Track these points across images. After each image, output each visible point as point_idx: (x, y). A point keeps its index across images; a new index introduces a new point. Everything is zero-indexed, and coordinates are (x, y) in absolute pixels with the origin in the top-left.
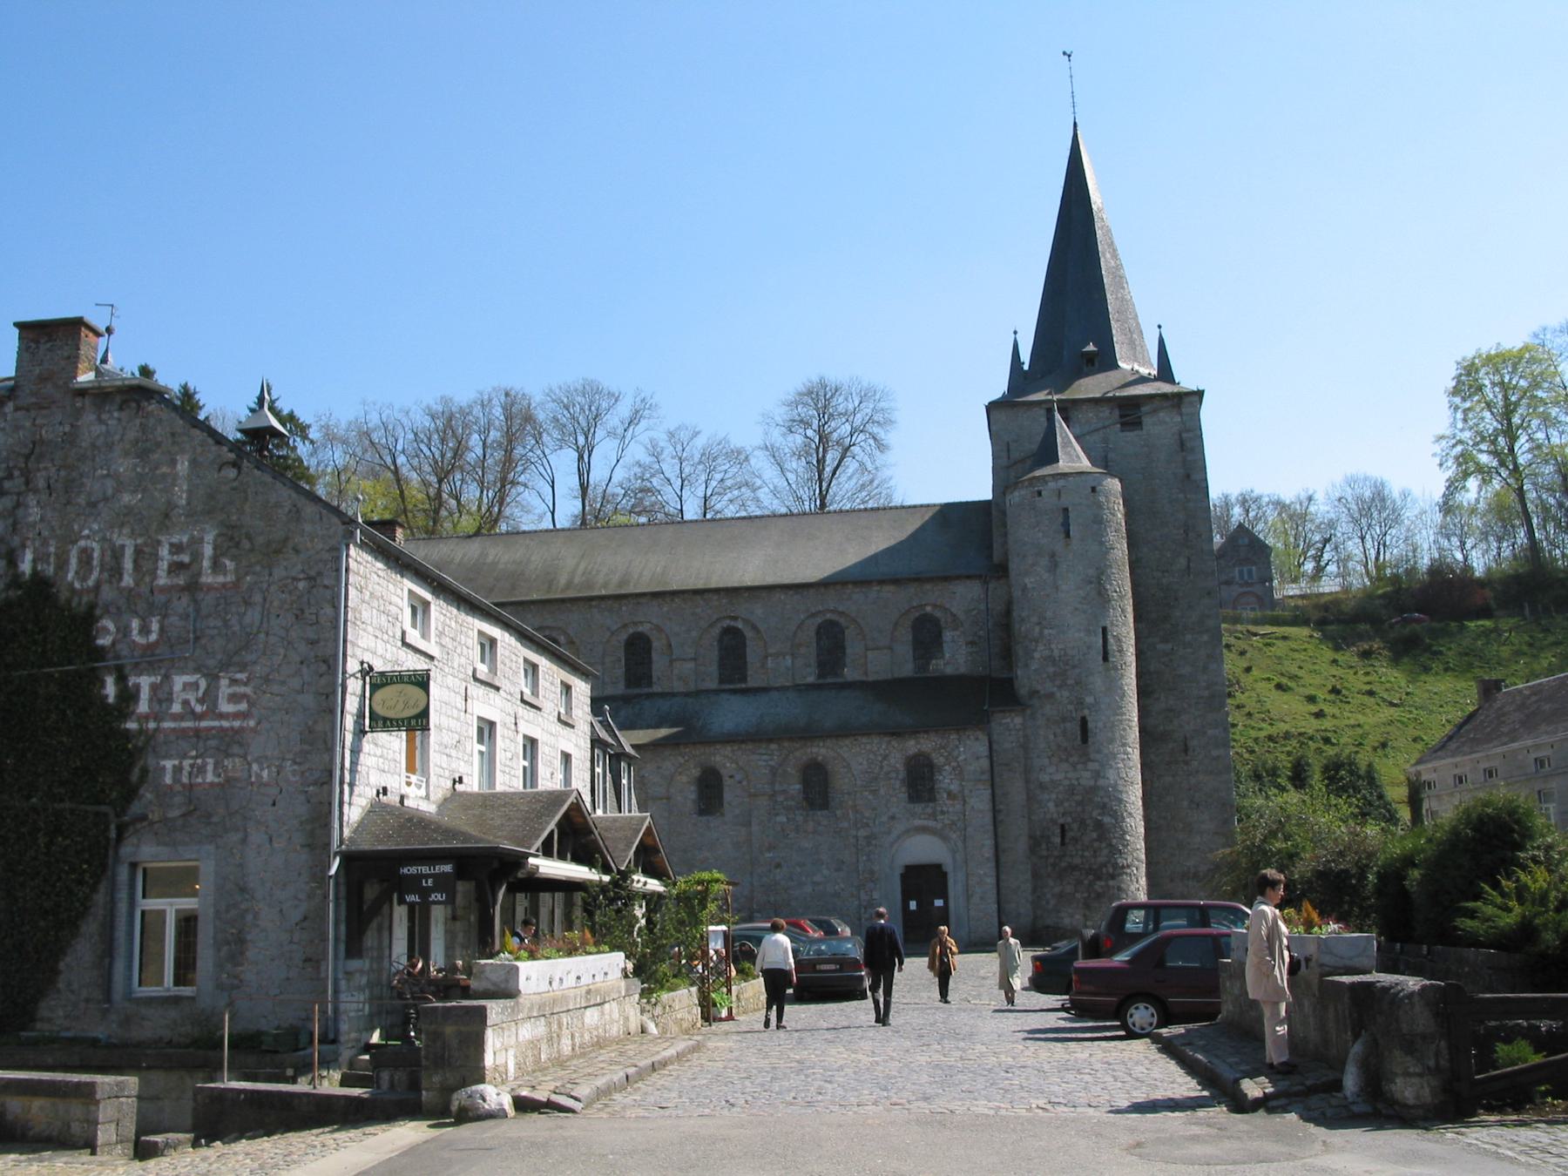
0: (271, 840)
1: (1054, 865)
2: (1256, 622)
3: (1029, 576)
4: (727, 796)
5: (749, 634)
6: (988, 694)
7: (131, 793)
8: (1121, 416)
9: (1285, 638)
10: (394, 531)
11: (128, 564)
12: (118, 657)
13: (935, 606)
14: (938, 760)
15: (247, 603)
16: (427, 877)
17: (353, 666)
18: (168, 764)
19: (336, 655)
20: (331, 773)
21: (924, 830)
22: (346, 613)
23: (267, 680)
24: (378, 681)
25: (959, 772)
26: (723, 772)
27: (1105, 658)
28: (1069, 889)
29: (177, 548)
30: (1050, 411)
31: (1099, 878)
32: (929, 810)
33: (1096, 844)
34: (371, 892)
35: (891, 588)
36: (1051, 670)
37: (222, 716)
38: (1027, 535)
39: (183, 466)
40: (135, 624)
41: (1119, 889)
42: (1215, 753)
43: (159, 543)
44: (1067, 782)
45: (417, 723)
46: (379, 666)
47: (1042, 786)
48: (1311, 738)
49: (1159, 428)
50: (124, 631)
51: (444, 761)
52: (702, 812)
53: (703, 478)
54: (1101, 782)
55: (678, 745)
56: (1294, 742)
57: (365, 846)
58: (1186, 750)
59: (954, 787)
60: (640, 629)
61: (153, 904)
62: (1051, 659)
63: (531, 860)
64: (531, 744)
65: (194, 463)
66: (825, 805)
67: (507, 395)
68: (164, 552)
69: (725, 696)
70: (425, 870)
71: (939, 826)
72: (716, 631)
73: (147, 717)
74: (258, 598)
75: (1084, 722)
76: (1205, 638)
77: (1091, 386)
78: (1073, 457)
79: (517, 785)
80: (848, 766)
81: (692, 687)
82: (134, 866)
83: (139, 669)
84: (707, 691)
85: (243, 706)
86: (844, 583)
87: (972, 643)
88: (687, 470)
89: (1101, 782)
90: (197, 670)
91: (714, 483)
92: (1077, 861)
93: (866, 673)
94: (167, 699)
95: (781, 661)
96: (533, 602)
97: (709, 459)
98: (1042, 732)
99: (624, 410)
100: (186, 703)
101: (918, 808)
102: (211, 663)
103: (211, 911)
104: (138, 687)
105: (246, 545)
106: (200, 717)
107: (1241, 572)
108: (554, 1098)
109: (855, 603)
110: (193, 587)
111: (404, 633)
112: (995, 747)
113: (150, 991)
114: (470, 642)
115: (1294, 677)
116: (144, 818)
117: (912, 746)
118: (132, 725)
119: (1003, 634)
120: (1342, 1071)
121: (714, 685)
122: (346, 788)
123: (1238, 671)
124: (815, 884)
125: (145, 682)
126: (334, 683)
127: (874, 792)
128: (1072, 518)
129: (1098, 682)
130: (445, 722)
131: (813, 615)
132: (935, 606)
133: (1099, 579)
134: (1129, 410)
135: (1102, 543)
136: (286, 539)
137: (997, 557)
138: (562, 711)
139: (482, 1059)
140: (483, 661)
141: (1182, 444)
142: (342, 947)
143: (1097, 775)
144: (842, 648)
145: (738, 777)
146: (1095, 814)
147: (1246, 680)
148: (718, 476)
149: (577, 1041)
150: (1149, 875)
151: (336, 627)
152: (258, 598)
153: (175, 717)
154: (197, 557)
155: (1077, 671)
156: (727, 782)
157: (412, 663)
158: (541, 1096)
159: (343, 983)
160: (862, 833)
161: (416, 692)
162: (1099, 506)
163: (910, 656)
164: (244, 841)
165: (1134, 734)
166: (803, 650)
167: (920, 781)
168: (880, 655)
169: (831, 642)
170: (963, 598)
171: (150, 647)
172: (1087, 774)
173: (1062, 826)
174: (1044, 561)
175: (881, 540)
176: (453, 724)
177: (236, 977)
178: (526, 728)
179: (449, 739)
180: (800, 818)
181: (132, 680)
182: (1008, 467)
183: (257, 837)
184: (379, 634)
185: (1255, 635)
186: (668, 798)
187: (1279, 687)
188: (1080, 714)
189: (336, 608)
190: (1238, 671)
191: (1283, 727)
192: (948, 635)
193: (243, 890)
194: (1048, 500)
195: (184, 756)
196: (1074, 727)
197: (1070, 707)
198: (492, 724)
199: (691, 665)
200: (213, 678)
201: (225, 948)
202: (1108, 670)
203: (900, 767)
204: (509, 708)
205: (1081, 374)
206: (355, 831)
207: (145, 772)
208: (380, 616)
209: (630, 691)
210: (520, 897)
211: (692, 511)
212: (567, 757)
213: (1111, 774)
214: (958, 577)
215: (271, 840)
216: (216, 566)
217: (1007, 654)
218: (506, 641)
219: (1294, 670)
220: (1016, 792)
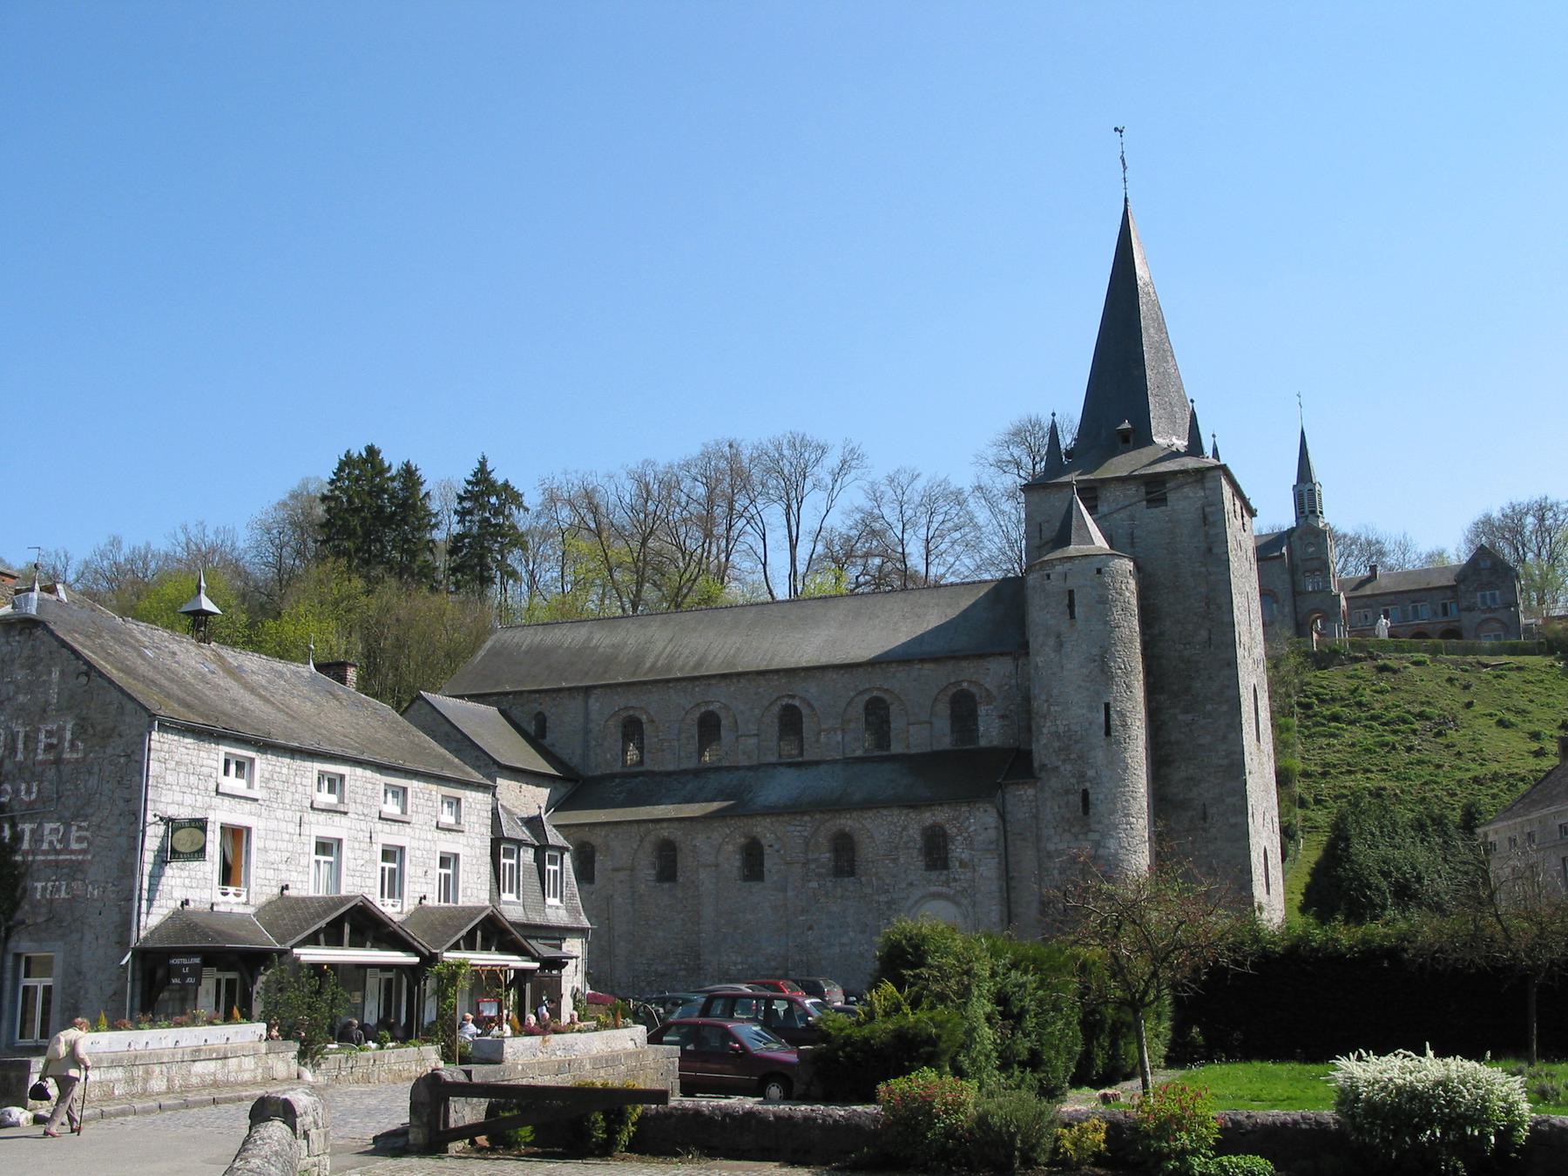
2: (1493, 652)
4: (767, 864)
5: (805, 711)
6: (1017, 763)
7: (16, 905)
8: (1147, 493)
9: (1520, 669)
11: (20, 746)
12: (12, 810)
13: (970, 682)
14: (951, 830)
15: (90, 773)
18: (39, 885)
23: (99, 826)
26: (763, 842)
27: (1108, 733)
29: (50, 734)
32: (943, 878)
35: (931, 666)
36: (1056, 744)
37: (72, 852)
38: (1042, 615)
39: (55, 675)
40: (23, 787)
42: (1232, 820)
43: (39, 730)
47: (1049, 856)
48: (1522, 780)
50: (16, 792)
52: (747, 878)
53: (924, 520)
54: (1101, 852)
55: (724, 817)
56: (1502, 784)
57: (150, 945)
58: (1205, 818)
61: (30, 982)
62: (1057, 736)
65: (62, 673)
66: (852, 873)
67: (731, 446)
68: (42, 736)
69: (782, 769)
70: (185, 961)
72: (776, 709)
73: (26, 853)
74: (96, 769)
75: (1085, 794)
76: (1225, 708)
77: (1122, 465)
80: (872, 837)
81: (754, 762)
82: (18, 956)
83: (24, 818)
84: (768, 765)
85: (85, 845)
86: (889, 663)
87: (1002, 717)
88: (909, 513)
89: (1101, 852)
90: (59, 820)
91: (935, 525)
94: (42, 839)
95: (835, 735)
96: (620, 685)
97: (929, 504)
99: (832, 460)
100: (51, 843)
101: (934, 875)
102: (67, 814)
104: (23, 831)
105: (91, 731)
106: (58, 853)
107: (1483, 597)
110: (58, 762)
113: (27, 1042)
115: (1521, 712)
116: (23, 922)
117: (928, 818)
118: (18, 858)
119: (1023, 712)
122: (144, 903)
123: (1456, 707)
124: (844, 945)
125: (27, 828)
126: (137, 831)
127: (895, 860)
128: (1083, 600)
129: (1099, 756)
131: (860, 693)
132: (970, 682)
133: (1103, 657)
134: (1155, 487)
135: (1106, 623)
136: (114, 729)
141: (1205, 518)
143: (1097, 845)
144: (888, 722)
147: (1463, 715)
148: (941, 518)
152: (96, 769)
153: (46, 853)
154: (61, 739)
156: (767, 851)
160: (883, 898)
161: (198, 833)
162: (1105, 587)
163: (947, 730)
164: (81, 939)
166: (852, 726)
167: (936, 851)
168: (921, 730)
169: (877, 713)
170: (994, 674)
171: (31, 803)
174: (1052, 642)
175: (933, 617)
181: (20, 826)
182: (1039, 547)
183: (89, 937)
185: (1486, 666)
186: (717, 866)
187: (1501, 723)
190: (1456, 707)
191: (1495, 767)
192: (982, 710)
193: (79, 973)
194: (1056, 583)
195: (48, 880)
196: (1076, 799)
199: (753, 741)
200: (68, 826)
202: (1110, 744)
205: (1114, 453)
206: (152, 933)
207: (25, 890)
211: (782, 592)
216: (73, 745)
219: (1522, 703)
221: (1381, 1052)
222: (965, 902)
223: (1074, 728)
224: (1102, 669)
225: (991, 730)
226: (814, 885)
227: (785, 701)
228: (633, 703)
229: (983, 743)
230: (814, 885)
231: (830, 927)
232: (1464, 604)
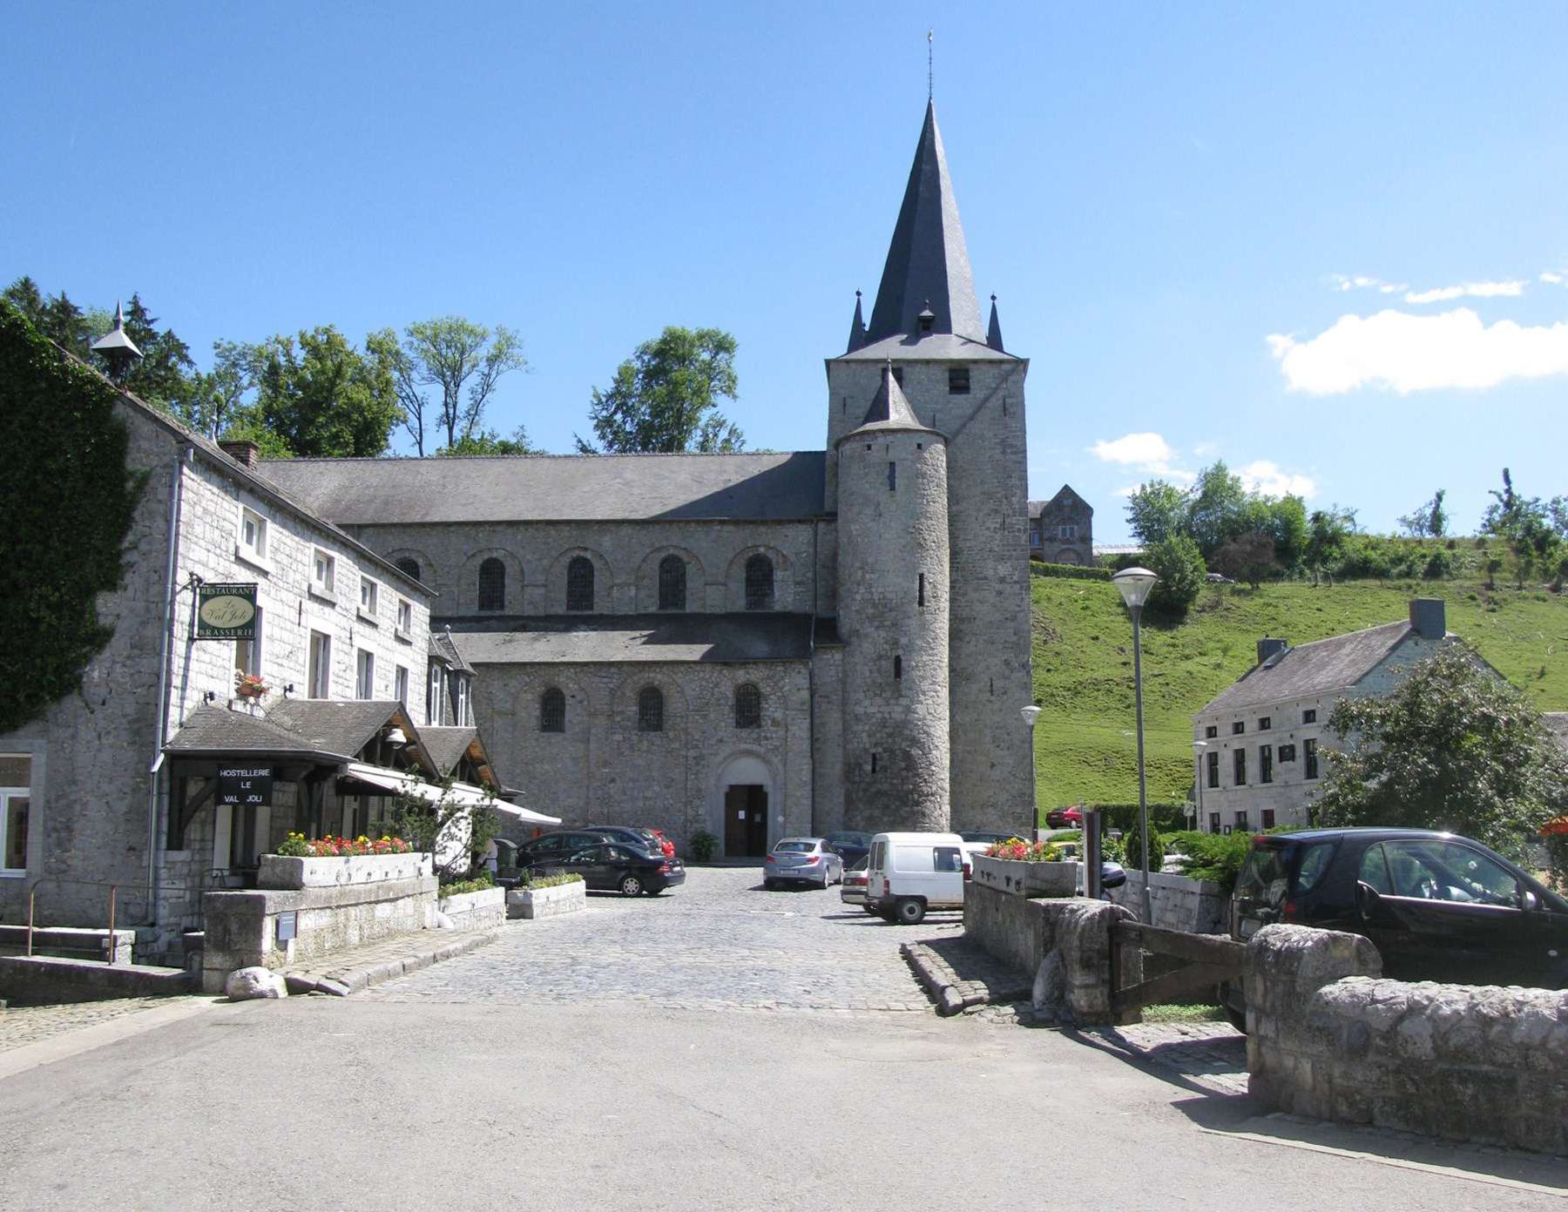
0: (99, 737)
1: (865, 790)
3: (856, 524)
4: (569, 715)
5: (597, 564)
6: (815, 630)
10: (248, 453)
14: (765, 689)
16: (246, 779)
17: (182, 578)
19: (167, 567)
20: (158, 676)
21: (749, 753)
22: (178, 527)
24: (207, 592)
25: (784, 699)
26: (565, 691)
27: (921, 603)
30: (885, 371)
31: (905, 804)
33: (904, 773)
34: (193, 789)
38: (859, 483)
41: (924, 815)
45: (247, 634)
46: (210, 578)
47: (857, 719)
49: (984, 396)
51: (275, 670)
59: (778, 715)
60: (495, 555)
63: (352, 766)
64: (366, 658)
66: (658, 727)
70: (244, 773)
71: (762, 750)
72: (566, 560)
75: (898, 660)
78: (900, 414)
79: (352, 694)
80: (682, 692)
81: (541, 612)
86: (671, 522)
92: (886, 787)
93: (704, 606)
99: (485, 350)
101: (744, 733)
103: (42, 801)
108: (324, 982)
111: (237, 548)
112: (816, 680)
114: (306, 560)
117: (741, 676)
119: (828, 573)
120: (1032, 981)
121: (561, 610)
124: (645, 798)
127: (704, 717)
129: (913, 623)
130: (277, 633)
131: (659, 550)
134: (959, 376)
137: (828, 506)
138: (401, 628)
139: (260, 945)
140: (319, 578)
142: (164, 838)
143: (908, 710)
145: (579, 698)
146: (904, 745)
149: (366, 932)
150: (953, 804)
151: (168, 540)
156: (569, 701)
157: (243, 576)
158: (312, 979)
159: (163, 873)
160: (692, 753)
161: (243, 604)
163: (742, 593)
164: (73, 737)
165: (943, 675)
166: (646, 582)
167: (748, 709)
170: (791, 544)
172: (900, 709)
173: (874, 755)
174: (869, 511)
176: (286, 636)
177: (64, 862)
178: (360, 642)
179: (283, 649)
180: (635, 738)
184: (210, 547)
189: (168, 522)
192: (778, 575)
196: (888, 665)
198: (327, 637)
199: (542, 591)
201: (54, 835)
204: (344, 622)
208: (208, 531)
209: (483, 613)
210: (349, 799)
212: (402, 673)
213: (921, 710)
214: (790, 522)
215: (99, 737)
217: (833, 596)
218: (343, 562)
220: (833, 722)
222: (775, 760)
223: (889, 596)
224: (918, 546)
225: (786, 595)
226: (618, 737)
227: (575, 554)
228: (409, 545)
230: (618, 737)
231: (634, 780)
232: (1046, 535)
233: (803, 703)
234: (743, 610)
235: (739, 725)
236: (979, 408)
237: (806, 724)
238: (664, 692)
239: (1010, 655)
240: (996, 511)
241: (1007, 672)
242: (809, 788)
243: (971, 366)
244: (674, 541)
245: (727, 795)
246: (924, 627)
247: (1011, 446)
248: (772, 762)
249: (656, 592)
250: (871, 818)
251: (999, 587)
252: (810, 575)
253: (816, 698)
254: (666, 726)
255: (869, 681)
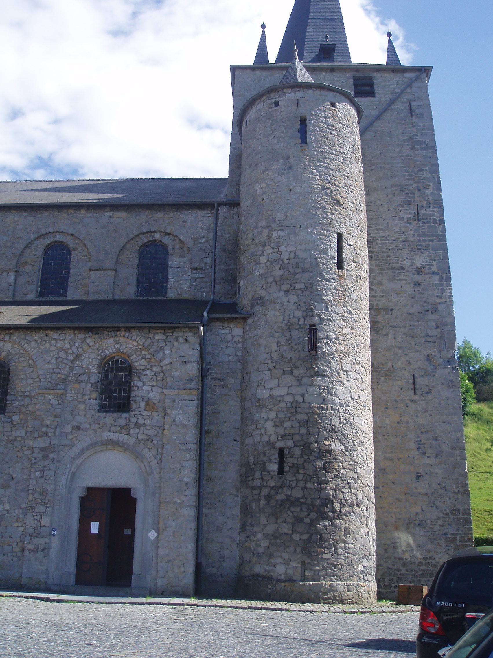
1: (268, 498)
14: (139, 363)
27: (340, 265)
28: (285, 529)
32: (122, 422)
41: (347, 532)
44: (289, 399)
47: (260, 404)
59: (154, 396)
71: (132, 441)
75: (313, 330)
92: (297, 493)
98: (262, 342)
101: (109, 418)
109: (90, 226)
117: (109, 345)
131: (42, 236)
155: (307, 275)
160: (40, 443)
163: (133, 280)
166: (28, 268)
167: (116, 391)
173: (281, 451)
188: (309, 322)
192: (174, 261)
197: (298, 314)
203: (94, 369)
217: (233, 280)
220: (229, 411)
221: (226, 599)
222: (148, 454)
223: (301, 255)
225: (181, 282)
229: (171, 295)
233: (191, 380)
234: (133, 297)
235: (104, 408)
236: (385, 110)
237: (192, 407)
238: (12, 366)
239: (433, 351)
240: (409, 203)
241: (430, 369)
242: (192, 491)
243: (375, 75)
244: (63, 226)
245: (83, 500)
246: (343, 292)
247: (420, 142)
248: (143, 458)
249: (36, 279)
250: (275, 536)
251: (417, 278)
252: (208, 260)
253: (208, 381)
254: (9, 407)
255: (276, 356)
